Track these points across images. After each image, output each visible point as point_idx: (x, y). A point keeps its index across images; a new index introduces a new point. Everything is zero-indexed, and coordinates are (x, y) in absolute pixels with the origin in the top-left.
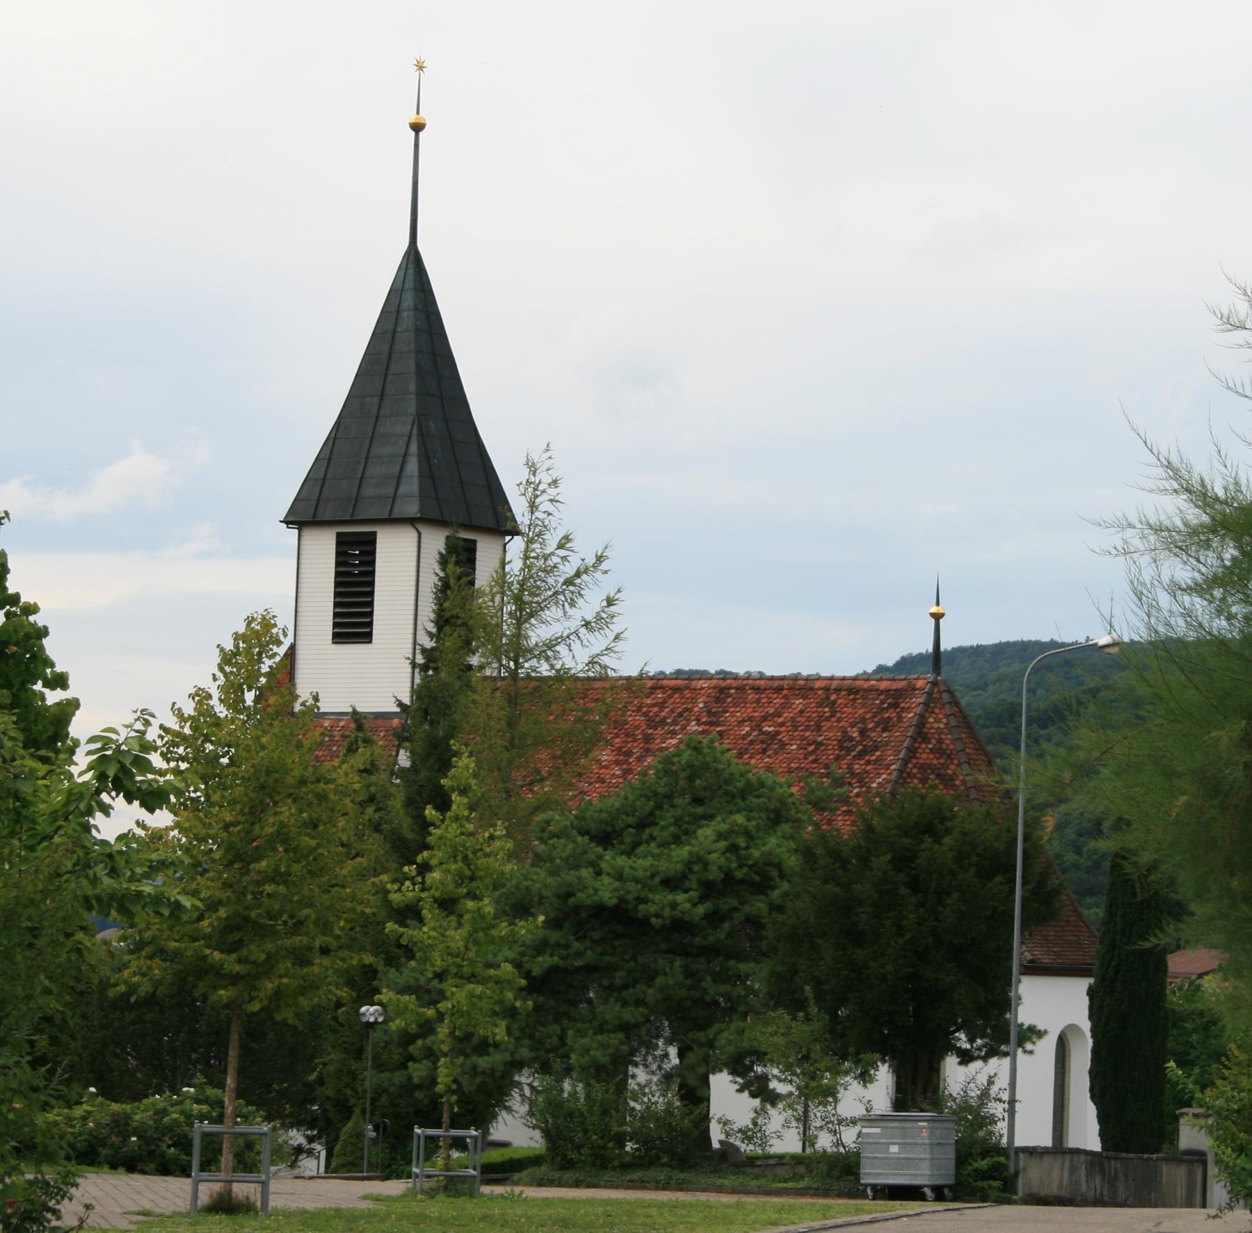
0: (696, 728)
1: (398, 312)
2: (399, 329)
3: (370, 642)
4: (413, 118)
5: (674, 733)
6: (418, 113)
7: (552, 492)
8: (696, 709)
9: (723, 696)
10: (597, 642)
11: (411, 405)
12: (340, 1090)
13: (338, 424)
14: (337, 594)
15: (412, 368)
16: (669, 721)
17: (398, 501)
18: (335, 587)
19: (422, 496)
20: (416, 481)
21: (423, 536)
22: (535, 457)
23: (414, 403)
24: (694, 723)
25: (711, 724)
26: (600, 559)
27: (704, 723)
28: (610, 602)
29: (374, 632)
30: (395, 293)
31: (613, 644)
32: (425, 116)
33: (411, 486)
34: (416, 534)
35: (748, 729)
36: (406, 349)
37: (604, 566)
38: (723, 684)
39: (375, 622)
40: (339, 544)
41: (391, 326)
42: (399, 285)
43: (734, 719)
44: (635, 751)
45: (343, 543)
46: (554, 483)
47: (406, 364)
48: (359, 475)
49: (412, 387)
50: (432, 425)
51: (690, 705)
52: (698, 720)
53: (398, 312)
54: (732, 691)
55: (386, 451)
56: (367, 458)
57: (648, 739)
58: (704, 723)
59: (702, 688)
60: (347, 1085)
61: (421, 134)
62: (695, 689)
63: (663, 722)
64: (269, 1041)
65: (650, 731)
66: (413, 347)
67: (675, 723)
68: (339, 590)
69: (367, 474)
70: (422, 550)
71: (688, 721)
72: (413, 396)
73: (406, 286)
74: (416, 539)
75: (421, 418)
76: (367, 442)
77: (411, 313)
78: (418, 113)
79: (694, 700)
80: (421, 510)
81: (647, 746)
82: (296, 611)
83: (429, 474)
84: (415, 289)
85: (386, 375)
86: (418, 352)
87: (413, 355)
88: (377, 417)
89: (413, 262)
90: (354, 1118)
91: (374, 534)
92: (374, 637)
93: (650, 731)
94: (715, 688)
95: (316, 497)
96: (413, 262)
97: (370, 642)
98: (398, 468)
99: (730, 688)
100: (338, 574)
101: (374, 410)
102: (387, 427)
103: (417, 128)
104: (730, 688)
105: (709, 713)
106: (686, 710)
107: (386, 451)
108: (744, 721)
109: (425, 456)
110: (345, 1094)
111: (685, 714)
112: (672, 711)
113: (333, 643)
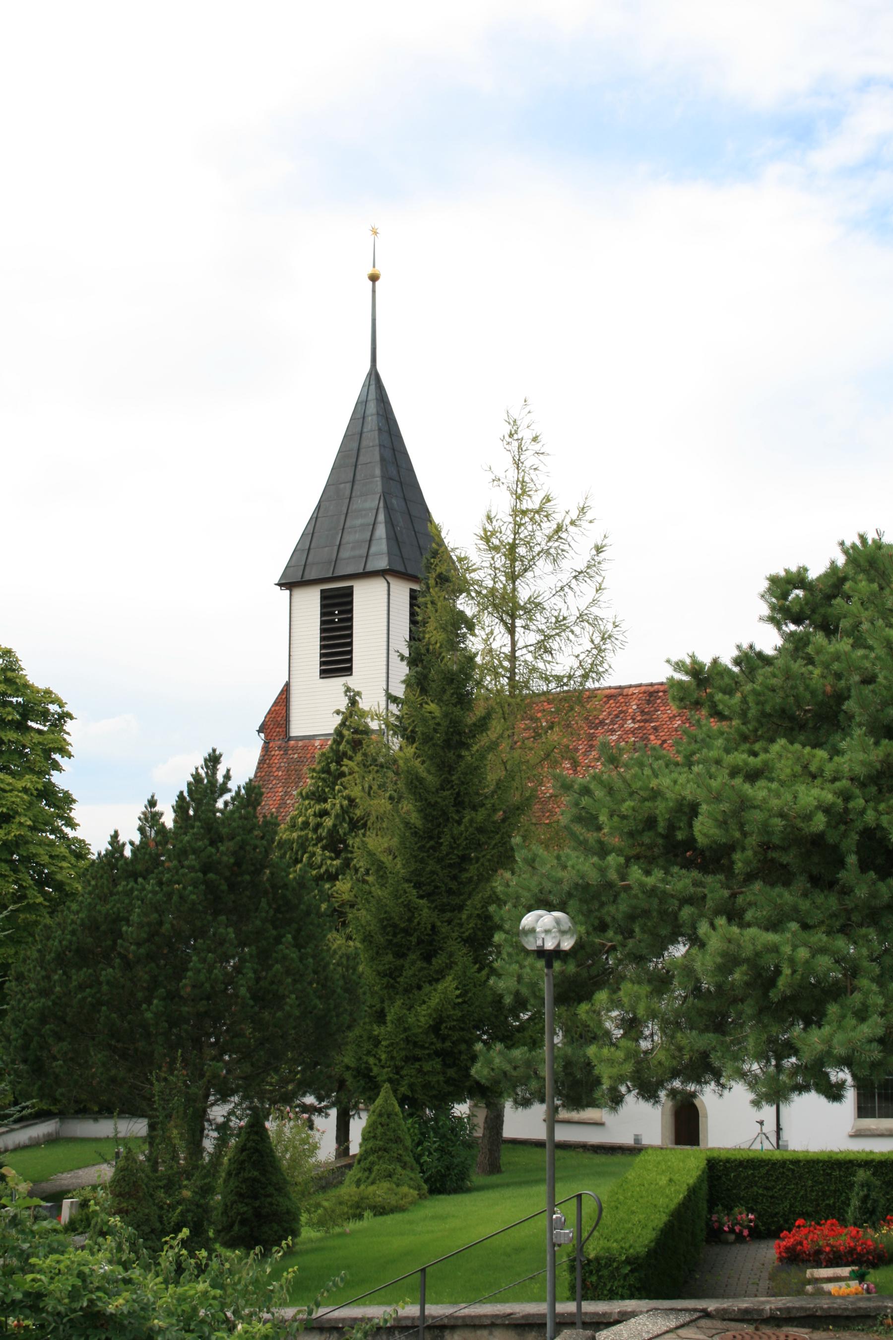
0: (632, 725)
1: (364, 418)
2: (365, 430)
3: (351, 675)
4: (370, 270)
5: (613, 731)
6: (374, 266)
7: (536, 447)
8: (630, 711)
9: (652, 698)
10: (587, 589)
11: (377, 486)
12: (360, 1058)
13: (319, 507)
14: (322, 639)
15: (377, 458)
16: (607, 721)
17: (370, 558)
18: (321, 617)
19: (389, 553)
20: (384, 542)
21: (391, 586)
22: (515, 414)
23: (379, 484)
24: (630, 721)
25: (645, 721)
26: (583, 510)
27: (638, 721)
28: (599, 549)
29: (354, 666)
30: (362, 404)
31: (597, 596)
32: (380, 269)
33: (381, 544)
34: (386, 584)
35: (679, 722)
36: (371, 444)
37: (589, 516)
38: (651, 689)
39: (354, 659)
40: (323, 598)
41: (359, 429)
42: (360, 415)
43: (666, 715)
44: (580, 747)
45: (325, 596)
46: (535, 439)
47: (372, 456)
48: (338, 543)
49: (378, 472)
50: (394, 501)
51: (625, 708)
52: (633, 719)
53: (364, 418)
54: (661, 694)
55: (359, 522)
56: (343, 529)
57: (592, 737)
58: (638, 721)
59: (633, 694)
60: (369, 1053)
61: (377, 283)
62: (627, 695)
63: (602, 723)
64: (287, 1008)
65: (592, 731)
66: (377, 442)
67: (613, 722)
68: (323, 659)
69: (344, 541)
70: (391, 597)
71: (625, 720)
72: (378, 479)
73: (369, 398)
74: (386, 588)
75: (386, 495)
76: (343, 517)
77: (375, 417)
78: (374, 266)
79: (627, 704)
80: (390, 563)
81: (590, 743)
82: (290, 655)
83: (394, 538)
84: (377, 399)
85: (356, 466)
86: (381, 446)
87: (377, 449)
88: (350, 498)
89: (374, 379)
90: (382, 1094)
91: (352, 587)
92: (354, 670)
93: (592, 731)
94: (645, 693)
95: (303, 563)
96: (374, 379)
97: (351, 675)
98: (369, 534)
99: (658, 692)
100: (323, 623)
101: (348, 492)
102: (357, 504)
103: (374, 278)
104: (658, 692)
105: (643, 712)
106: (621, 712)
107: (359, 522)
108: (675, 716)
109: (391, 524)
110: (366, 1063)
111: (621, 716)
112: (609, 713)
113: (321, 678)
